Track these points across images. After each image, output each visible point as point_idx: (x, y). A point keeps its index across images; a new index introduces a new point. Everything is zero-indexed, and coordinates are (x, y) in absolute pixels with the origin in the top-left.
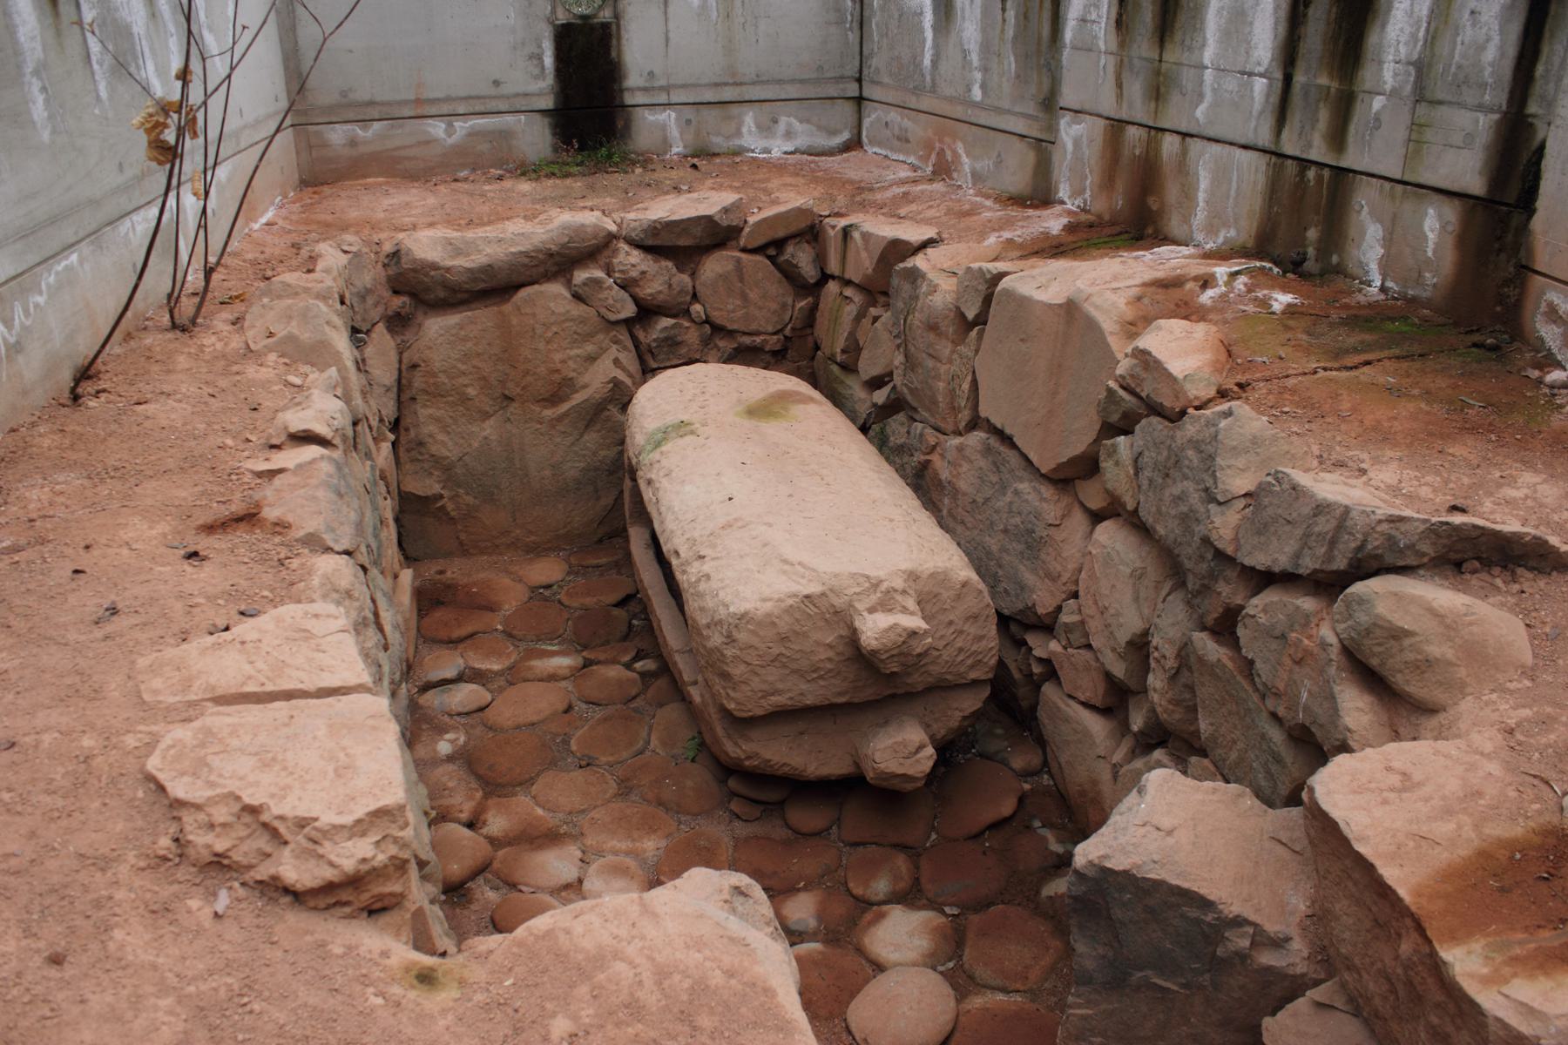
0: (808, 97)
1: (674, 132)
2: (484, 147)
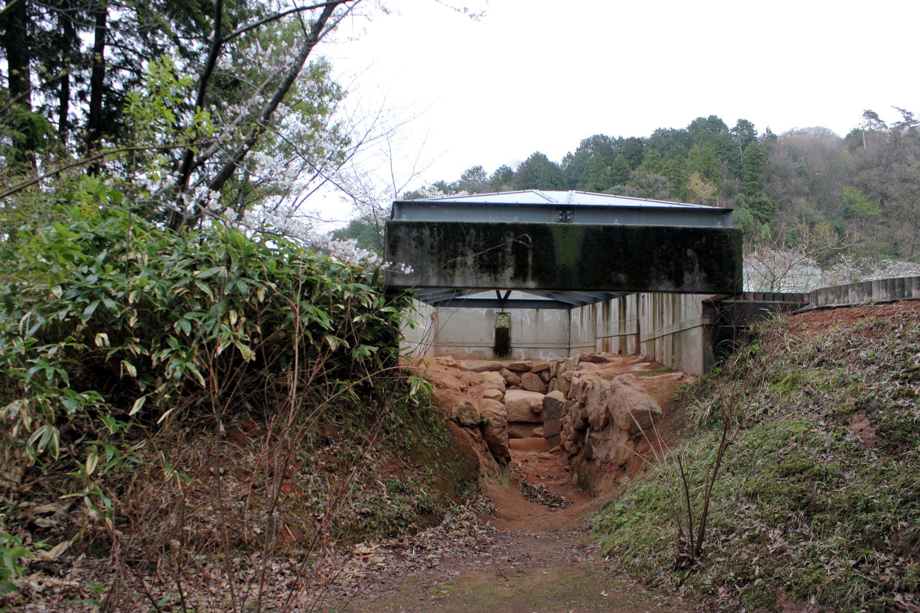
0: (557, 348)
1: (523, 354)
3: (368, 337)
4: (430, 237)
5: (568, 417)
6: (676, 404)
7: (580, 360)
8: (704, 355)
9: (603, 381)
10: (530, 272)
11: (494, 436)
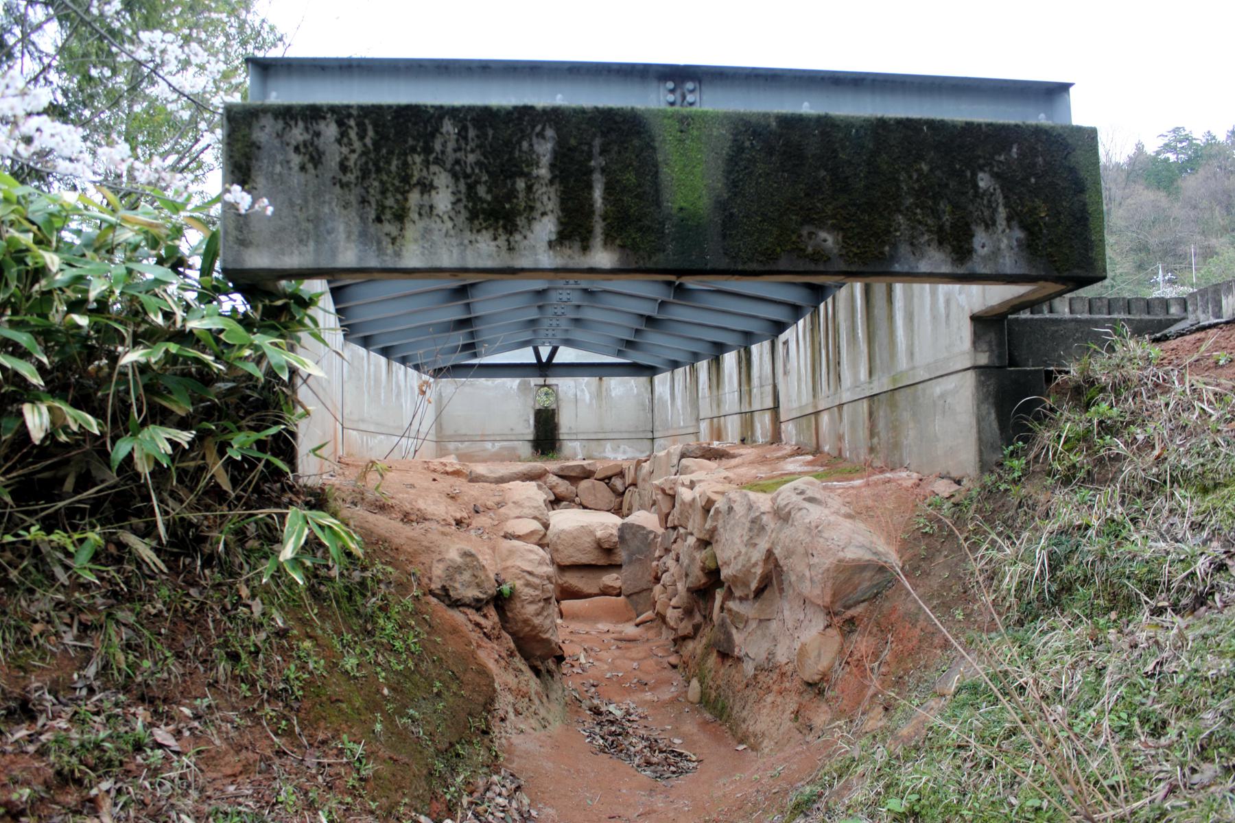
1: (579, 450)
2: (506, 453)
3: (182, 408)
4: (339, 141)
5: (669, 561)
6: (934, 539)
7: (683, 456)
8: (979, 432)
9: (753, 495)
10: (599, 227)
11: (526, 622)
